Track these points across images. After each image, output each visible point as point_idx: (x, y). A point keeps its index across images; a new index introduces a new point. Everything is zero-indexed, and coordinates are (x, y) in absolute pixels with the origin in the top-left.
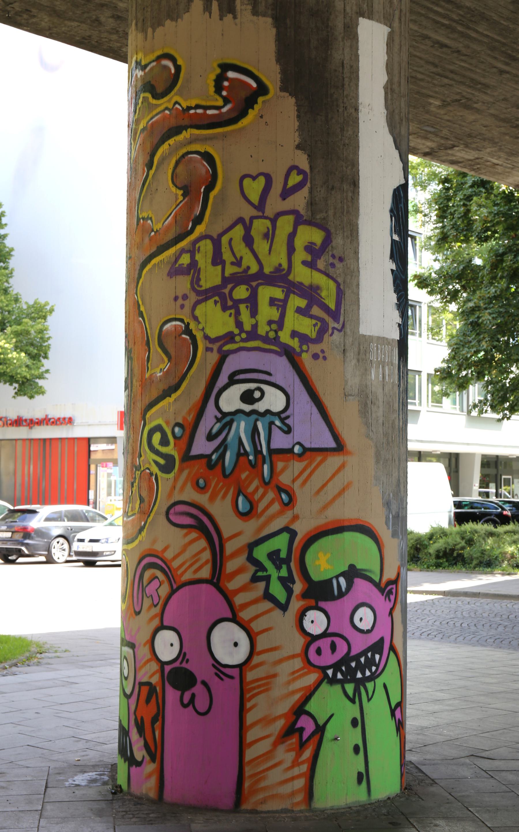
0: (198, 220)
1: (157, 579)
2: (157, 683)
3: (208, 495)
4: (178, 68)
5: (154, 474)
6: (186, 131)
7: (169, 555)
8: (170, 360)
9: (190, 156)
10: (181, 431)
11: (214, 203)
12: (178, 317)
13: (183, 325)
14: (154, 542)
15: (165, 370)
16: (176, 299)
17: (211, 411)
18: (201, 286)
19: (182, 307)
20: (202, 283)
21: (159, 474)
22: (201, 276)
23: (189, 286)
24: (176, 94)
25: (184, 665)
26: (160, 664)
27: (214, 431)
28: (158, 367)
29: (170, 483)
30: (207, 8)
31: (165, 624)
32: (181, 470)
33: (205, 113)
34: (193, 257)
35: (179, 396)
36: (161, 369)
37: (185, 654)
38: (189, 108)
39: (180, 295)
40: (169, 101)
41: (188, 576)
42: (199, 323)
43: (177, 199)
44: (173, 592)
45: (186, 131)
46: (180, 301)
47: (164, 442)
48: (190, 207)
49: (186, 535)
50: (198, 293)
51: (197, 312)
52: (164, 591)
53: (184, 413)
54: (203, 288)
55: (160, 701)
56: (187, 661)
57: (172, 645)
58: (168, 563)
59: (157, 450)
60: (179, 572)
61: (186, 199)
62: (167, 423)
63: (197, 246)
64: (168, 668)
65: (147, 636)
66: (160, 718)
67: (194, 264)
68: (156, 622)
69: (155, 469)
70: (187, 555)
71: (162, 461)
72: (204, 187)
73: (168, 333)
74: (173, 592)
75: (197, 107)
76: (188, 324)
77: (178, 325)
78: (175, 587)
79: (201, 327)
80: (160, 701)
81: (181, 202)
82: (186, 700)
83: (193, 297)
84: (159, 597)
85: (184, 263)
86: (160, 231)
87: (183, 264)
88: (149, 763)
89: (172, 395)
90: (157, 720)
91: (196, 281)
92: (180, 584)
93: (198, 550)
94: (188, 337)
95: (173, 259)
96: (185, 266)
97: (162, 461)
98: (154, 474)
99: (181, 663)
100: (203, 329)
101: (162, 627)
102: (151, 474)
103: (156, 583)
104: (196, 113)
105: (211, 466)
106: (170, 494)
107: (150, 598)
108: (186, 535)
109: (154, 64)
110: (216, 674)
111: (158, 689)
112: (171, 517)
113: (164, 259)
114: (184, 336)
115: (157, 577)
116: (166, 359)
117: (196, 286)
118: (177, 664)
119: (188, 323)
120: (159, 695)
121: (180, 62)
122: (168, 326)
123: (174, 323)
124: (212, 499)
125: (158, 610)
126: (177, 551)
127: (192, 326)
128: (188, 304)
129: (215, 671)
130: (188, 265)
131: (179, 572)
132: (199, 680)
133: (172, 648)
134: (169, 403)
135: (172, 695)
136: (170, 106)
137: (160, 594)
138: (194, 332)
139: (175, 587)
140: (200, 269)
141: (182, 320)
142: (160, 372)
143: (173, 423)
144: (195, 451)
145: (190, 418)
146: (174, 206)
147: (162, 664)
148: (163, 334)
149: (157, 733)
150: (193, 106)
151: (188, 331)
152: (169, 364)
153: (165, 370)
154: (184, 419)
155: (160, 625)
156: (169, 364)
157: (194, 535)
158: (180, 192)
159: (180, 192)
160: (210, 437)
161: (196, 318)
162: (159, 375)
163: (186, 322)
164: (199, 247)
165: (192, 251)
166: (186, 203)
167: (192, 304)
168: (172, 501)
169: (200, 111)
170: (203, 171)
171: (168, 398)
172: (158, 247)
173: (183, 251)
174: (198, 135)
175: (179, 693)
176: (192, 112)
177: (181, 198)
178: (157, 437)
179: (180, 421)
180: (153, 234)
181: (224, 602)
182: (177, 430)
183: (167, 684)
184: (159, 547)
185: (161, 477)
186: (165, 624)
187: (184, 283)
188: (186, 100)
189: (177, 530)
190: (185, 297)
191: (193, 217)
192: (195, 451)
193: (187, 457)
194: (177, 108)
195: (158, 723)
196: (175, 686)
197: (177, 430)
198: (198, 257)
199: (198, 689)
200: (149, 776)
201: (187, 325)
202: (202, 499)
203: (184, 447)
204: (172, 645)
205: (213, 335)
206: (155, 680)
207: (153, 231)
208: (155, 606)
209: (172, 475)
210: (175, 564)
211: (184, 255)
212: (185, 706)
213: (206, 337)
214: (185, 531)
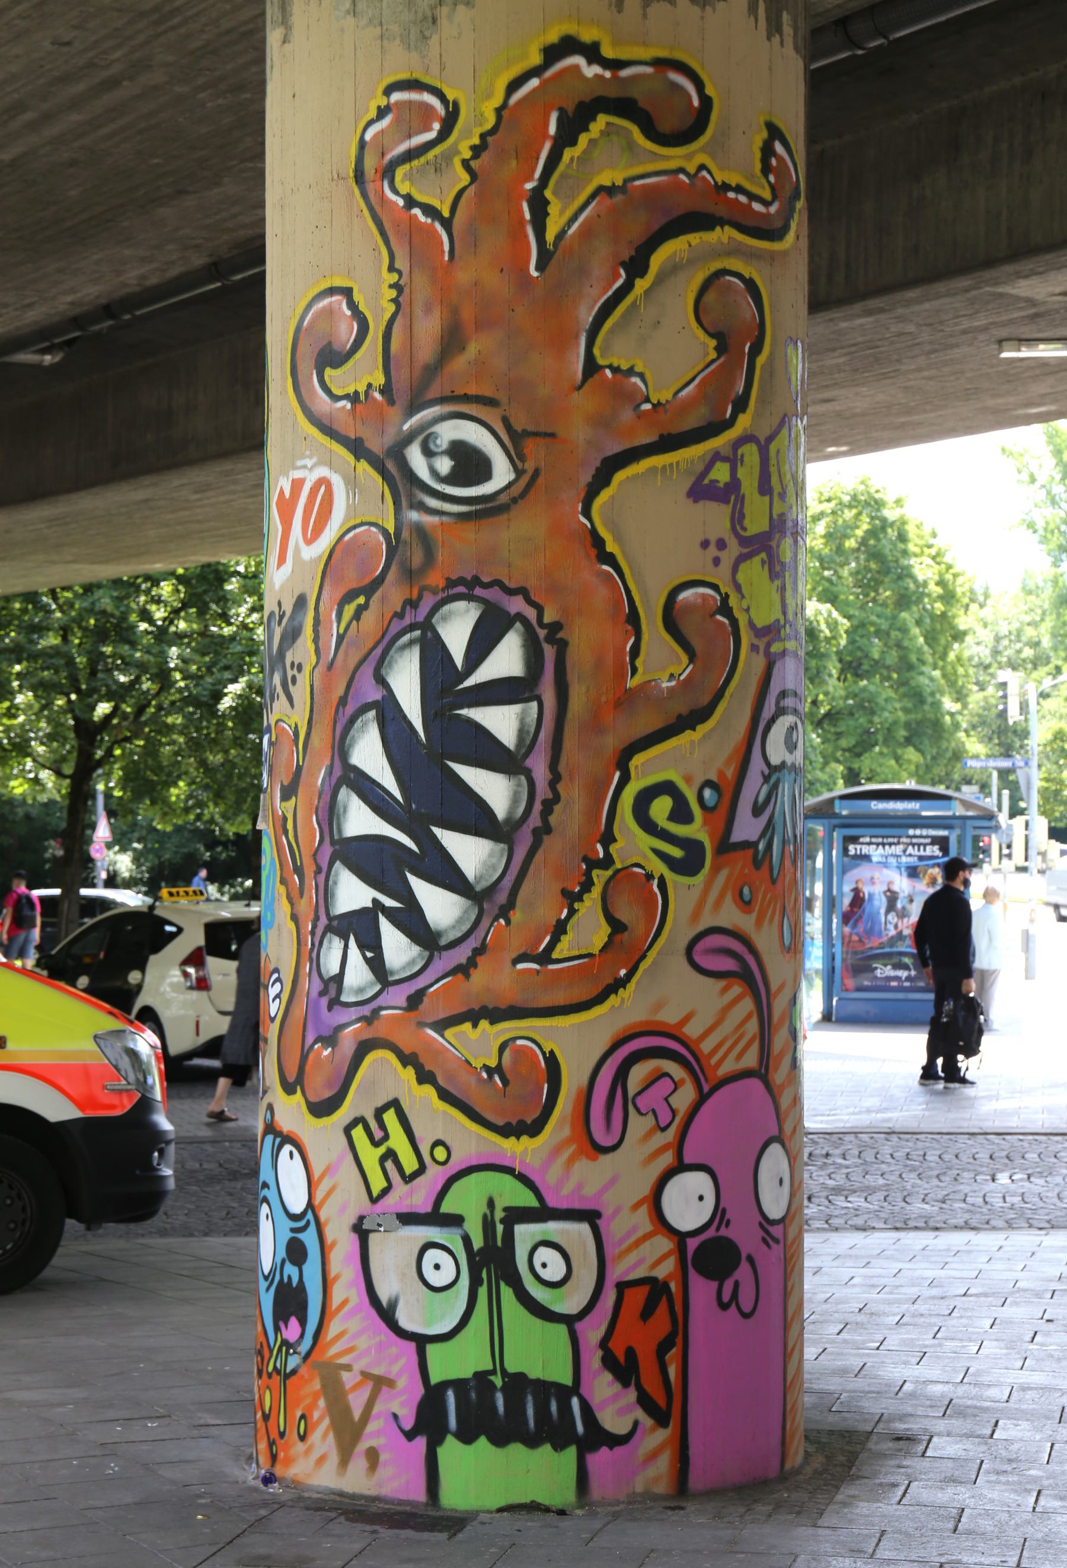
0: (741, 404)
1: (667, 1079)
2: (670, 1276)
3: (754, 915)
4: (706, 102)
5: (657, 875)
6: (722, 228)
7: (692, 1031)
8: (691, 660)
9: (728, 278)
10: (716, 795)
11: (761, 378)
12: (708, 579)
13: (718, 598)
14: (659, 1007)
15: (682, 678)
16: (705, 544)
17: (757, 765)
18: (745, 529)
19: (716, 561)
20: (747, 523)
21: (670, 876)
22: (745, 511)
23: (728, 525)
24: (703, 150)
25: (724, 1232)
26: (676, 1239)
27: (761, 799)
28: (663, 669)
29: (695, 895)
30: (753, 9)
31: (687, 1160)
32: (716, 869)
33: (750, 205)
34: (733, 471)
35: (712, 730)
36: (672, 676)
37: (724, 1211)
38: (726, 187)
39: (713, 539)
40: (689, 157)
41: (728, 1067)
42: (743, 597)
43: (707, 354)
44: (702, 1098)
45: (722, 228)
46: (712, 551)
47: (681, 813)
48: (726, 374)
49: (724, 990)
50: (743, 541)
51: (740, 577)
52: (684, 1098)
53: (719, 763)
54: (747, 534)
55: (678, 1308)
56: (727, 1225)
57: (701, 1198)
58: (693, 1046)
59: (663, 830)
60: (713, 1061)
61: (722, 360)
62: (688, 780)
63: (740, 452)
64: (692, 1244)
65: (645, 1188)
66: (679, 1340)
67: (734, 484)
68: (667, 1159)
69: (659, 867)
70: (728, 1026)
71: (677, 853)
72: (748, 344)
73: (689, 607)
74: (702, 1098)
75: (739, 189)
76: (727, 596)
77: (710, 596)
78: (706, 1088)
79: (744, 605)
80: (678, 1308)
81: (713, 361)
82: (726, 1297)
83: (734, 549)
84: (674, 1112)
85: (719, 479)
86: (667, 407)
87: (717, 481)
88: (653, 1430)
89: (699, 727)
90: (672, 1345)
91: (738, 519)
92: (717, 1081)
93: (741, 1019)
94: (726, 621)
95: (700, 468)
96: (721, 485)
97: (677, 853)
98: (657, 875)
99: (718, 1229)
100: (748, 610)
101: (680, 1167)
102: (649, 877)
103: (665, 1085)
104: (737, 199)
105: (757, 864)
106: (696, 916)
107: (650, 1115)
108: (724, 990)
109: (649, 70)
110: (764, 1240)
111: (673, 1286)
112: (697, 958)
113: (678, 463)
114: (719, 617)
115: (667, 1075)
116: (684, 658)
117: (738, 528)
118: (711, 1233)
119: (726, 594)
120: (675, 1297)
121: (709, 91)
122: (684, 595)
123: (702, 590)
124: (759, 923)
125: (670, 1135)
126: (710, 1022)
127: (733, 602)
128: (728, 557)
129: (762, 1234)
130: (726, 484)
131: (713, 1061)
132: (744, 1256)
133: (701, 1203)
134: (692, 742)
135: (702, 1290)
136: (691, 169)
137: (674, 1107)
138: (737, 614)
139: (706, 1088)
140: (744, 495)
141: (715, 587)
142: (669, 680)
143: (699, 781)
144: (738, 835)
145: (730, 773)
146: (701, 366)
147: (680, 1237)
148: (677, 606)
149: (672, 1371)
150: (734, 185)
151: (725, 609)
152: (691, 667)
153: (682, 678)
154: (721, 774)
155: (676, 1164)
156: (691, 667)
157: (737, 990)
158: (713, 343)
159: (713, 343)
160: (757, 811)
161: (738, 588)
162: (665, 685)
163: (723, 591)
164: (742, 456)
165: (734, 461)
166: (721, 365)
167: (733, 560)
168: (702, 926)
169: (743, 199)
170: (748, 315)
171: (688, 732)
172: (661, 436)
173: (717, 456)
174: (740, 243)
175: (715, 1285)
176: (731, 195)
177: (713, 355)
178: (661, 808)
179: (714, 777)
180: (647, 406)
181: (697, 1119)
182: (707, 793)
183: (692, 1272)
184: (670, 1016)
185: (675, 883)
186: (687, 1160)
187: (715, 518)
188: (721, 169)
189: (710, 981)
190: (721, 544)
191: (733, 396)
192: (738, 835)
193: (725, 846)
194: (704, 178)
195: (674, 1350)
196: (707, 1273)
197: (707, 793)
198: (741, 473)
199: (743, 1272)
200: (653, 1455)
201: (725, 598)
202: (745, 922)
203: (721, 825)
204: (701, 1198)
205: (760, 624)
206: (665, 1270)
207: (647, 400)
208: (663, 1129)
209: (700, 879)
210: (706, 1047)
211: (719, 465)
212: (724, 1307)
213: (751, 624)
214: (722, 983)
